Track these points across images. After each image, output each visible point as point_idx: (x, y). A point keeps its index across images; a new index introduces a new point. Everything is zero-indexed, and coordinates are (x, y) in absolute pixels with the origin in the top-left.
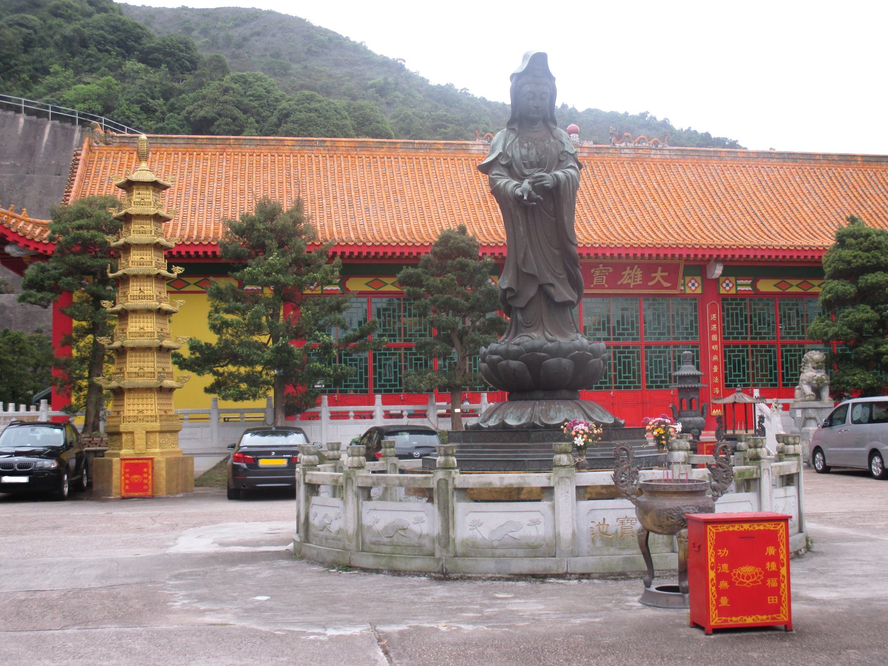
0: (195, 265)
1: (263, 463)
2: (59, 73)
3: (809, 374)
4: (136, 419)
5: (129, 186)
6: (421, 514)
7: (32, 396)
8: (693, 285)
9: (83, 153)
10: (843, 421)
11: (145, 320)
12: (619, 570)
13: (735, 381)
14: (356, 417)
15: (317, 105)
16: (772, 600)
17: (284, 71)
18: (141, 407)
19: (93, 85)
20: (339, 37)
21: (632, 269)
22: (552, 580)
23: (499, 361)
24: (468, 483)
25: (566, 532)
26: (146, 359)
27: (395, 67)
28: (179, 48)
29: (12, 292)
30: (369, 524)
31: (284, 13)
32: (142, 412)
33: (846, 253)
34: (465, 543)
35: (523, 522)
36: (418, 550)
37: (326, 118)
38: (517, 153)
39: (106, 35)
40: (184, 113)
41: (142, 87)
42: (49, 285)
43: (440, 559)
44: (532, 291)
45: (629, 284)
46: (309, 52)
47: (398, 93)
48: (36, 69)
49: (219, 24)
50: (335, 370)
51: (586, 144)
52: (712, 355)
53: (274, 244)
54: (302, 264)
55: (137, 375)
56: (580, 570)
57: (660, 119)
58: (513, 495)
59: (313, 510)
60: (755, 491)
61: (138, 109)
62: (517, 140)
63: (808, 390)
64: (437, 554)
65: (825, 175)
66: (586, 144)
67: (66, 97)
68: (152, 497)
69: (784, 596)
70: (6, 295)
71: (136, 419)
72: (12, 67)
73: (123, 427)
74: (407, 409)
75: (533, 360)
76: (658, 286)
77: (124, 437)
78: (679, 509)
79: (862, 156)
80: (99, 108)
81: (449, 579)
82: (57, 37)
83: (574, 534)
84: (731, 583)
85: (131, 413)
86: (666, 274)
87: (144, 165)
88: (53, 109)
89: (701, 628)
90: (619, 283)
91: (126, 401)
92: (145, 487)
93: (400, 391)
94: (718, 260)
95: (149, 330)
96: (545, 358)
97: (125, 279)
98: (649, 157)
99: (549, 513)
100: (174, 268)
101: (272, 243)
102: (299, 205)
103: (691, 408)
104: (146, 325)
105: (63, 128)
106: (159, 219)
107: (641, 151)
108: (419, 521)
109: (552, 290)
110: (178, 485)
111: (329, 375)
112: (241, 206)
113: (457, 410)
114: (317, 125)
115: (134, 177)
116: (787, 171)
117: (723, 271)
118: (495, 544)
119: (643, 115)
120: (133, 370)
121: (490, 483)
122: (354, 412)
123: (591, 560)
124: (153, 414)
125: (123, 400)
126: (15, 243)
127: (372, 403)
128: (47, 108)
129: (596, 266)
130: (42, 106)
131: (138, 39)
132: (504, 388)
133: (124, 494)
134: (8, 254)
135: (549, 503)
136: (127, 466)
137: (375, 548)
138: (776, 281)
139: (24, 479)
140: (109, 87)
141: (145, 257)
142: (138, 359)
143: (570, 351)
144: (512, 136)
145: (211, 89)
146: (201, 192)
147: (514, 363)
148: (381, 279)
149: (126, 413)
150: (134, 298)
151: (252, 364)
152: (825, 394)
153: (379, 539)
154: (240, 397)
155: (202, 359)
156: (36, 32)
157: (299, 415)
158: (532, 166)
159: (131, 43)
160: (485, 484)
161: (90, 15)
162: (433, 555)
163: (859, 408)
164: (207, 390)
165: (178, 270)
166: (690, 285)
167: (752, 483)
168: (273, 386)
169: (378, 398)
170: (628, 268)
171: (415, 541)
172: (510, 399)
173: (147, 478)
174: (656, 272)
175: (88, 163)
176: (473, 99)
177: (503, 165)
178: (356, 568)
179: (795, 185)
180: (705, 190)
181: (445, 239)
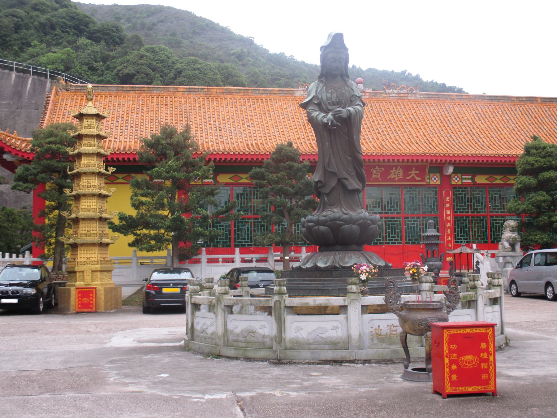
0: (122, 167)
1: (165, 290)
2: (37, 46)
3: (507, 234)
4: (86, 263)
5: (81, 117)
6: (264, 323)
7: (20, 249)
8: (435, 179)
9: (52, 96)
10: (529, 264)
11: (91, 201)
12: (388, 358)
13: (461, 239)
14: (223, 262)
15: (199, 66)
16: (484, 377)
17: (178, 45)
18: (88, 256)
19: (58, 53)
20: (213, 23)
21: (396, 169)
22: (346, 364)
23: (313, 226)
24: (294, 303)
25: (355, 334)
26: (92, 225)
27: (248, 42)
28: (112, 30)
29: (7, 183)
30: (232, 329)
31: (178, 8)
32: (89, 258)
33: (531, 159)
34: (291, 341)
35: (328, 328)
36: (262, 345)
37: (205, 74)
38: (324, 96)
39: (67, 22)
40: (115, 71)
41: (89, 54)
42: (31, 179)
43: (276, 351)
44: (334, 183)
45: (395, 178)
46: (194, 32)
47: (249, 58)
48: (23, 44)
49: (138, 15)
50: (210, 232)
51: (368, 90)
52: (447, 223)
53: (172, 153)
54: (190, 165)
55: (86, 235)
56: (364, 358)
57: (414, 74)
58: (322, 311)
59: (196, 320)
60: (473, 308)
61: (87, 69)
62: (324, 88)
63: (507, 245)
64: (274, 348)
65: (518, 110)
66: (368, 90)
67: (41, 61)
68: (95, 312)
69: (492, 374)
70: (4, 185)
71: (86, 263)
72: (8, 42)
73: (77, 268)
74: (255, 256)
75: (334, 226)
76: (413, 179)
77: (78, 274)
78: (426, 319)
79: (541, 98)
80: (62, 67)
81: (282, 363)
82: (36, 23)
83: (360, 335)
84: (458, 366)
85: (82, 260)
86: (418, 172)
87: (90, 104)
88: (33, 68)
89: (440, 394)
90: (388, 178)
91: (79, 252)
92: (91, 306)
93: (251, 245)
94: (450, 163)
95: (94, 207)
96: (342, 225)
97: (78, 175)
98: (407, 99)
99: (344, 322)
100: (109, 168)
101: (171, 153)
102: (187, 129)
103: (433, 256)
104: (91, 204)
105: (40, 80)
106: (99, 137)
107: (402, 95)
108: (263, 327)
109: (346, 182)
110: (111, 305)
111: (206, 236)
112: (151, 129)
113: (287, 258)
114: (199, 78)
115: (84, 111)
116: (494, 107)
117: (454, 170)
118: (311, 341)
119: (404, 72)
120: (83, 232)
121: (308, 303)
122: (222, 259)
123: (371, 351)
124: (96, 260)
125: (77, 251)
126: (10, 152)
127: (233, 253)
128: (30, 68)
129: (374, 167)
130: (26, 67)
131: (87, 25)
132: (316, 243)
133: (78, 310)
134: (5, 160)
135: (345, 316)
136: (79, 292)
137: (235, 344)
138: (487, 177)
139: (15, 301)
140: (68, 55)
141: (91, 161)
142: (86, 225)
143: (357, 220)
144: (321, 85)
145: (132, 56)
146: (126, 120)
147: (322, 228)
148: (239, 175)
149: (79, 259)
150: (84, 187)
151: (158, 228)
152: (518, 247)
153: (238, 338)
154: (151, 249)
155: (127, 225)
156: (22, 20)
157: (187, 261)
158: (334, 104)
159: (82, 27)
160: (304, 304)
161: (56, 9)
162: (271, 348)
163: (539, 256)
164: (130, 245)
165: (112, 169)
166: (433, 179)
167: (472, 303)
168: (171, 242)
169: (237, 250)
170: (394, 168)
171: (260, 339)
172: (320, 250)
173: (92, 300)
174: (412, 171)
175: (55, 103)
176: (297, 62)
177: (315, 104)
178: (223, 356)
179: (499, 116)
180: (442, 119)
181: (279, 150)
